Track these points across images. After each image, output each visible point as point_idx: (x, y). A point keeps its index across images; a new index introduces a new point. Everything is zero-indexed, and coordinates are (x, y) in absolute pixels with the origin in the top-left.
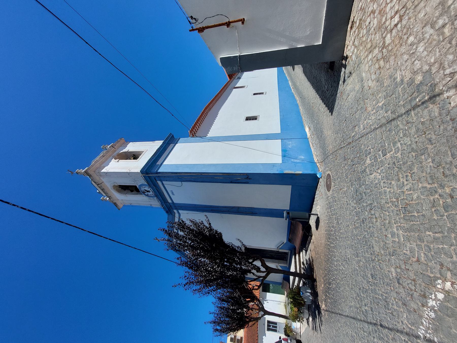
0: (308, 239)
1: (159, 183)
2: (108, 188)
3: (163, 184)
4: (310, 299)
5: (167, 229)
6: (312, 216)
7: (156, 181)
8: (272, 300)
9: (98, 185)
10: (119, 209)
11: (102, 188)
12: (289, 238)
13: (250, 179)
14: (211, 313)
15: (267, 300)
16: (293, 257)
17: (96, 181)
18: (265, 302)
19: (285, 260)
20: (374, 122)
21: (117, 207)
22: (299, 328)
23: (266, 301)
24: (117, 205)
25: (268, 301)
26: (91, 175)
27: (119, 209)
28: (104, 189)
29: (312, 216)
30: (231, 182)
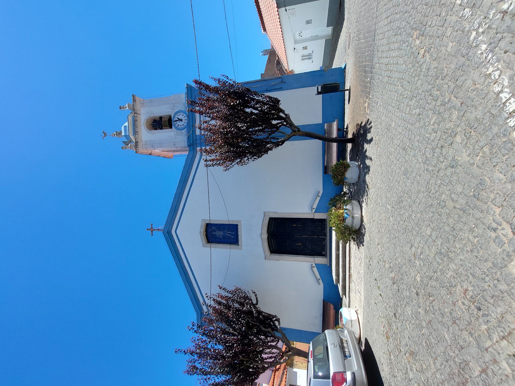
10: (136, 152)
11: (136, 119)
17: (136, 109)
24: (138, 145)
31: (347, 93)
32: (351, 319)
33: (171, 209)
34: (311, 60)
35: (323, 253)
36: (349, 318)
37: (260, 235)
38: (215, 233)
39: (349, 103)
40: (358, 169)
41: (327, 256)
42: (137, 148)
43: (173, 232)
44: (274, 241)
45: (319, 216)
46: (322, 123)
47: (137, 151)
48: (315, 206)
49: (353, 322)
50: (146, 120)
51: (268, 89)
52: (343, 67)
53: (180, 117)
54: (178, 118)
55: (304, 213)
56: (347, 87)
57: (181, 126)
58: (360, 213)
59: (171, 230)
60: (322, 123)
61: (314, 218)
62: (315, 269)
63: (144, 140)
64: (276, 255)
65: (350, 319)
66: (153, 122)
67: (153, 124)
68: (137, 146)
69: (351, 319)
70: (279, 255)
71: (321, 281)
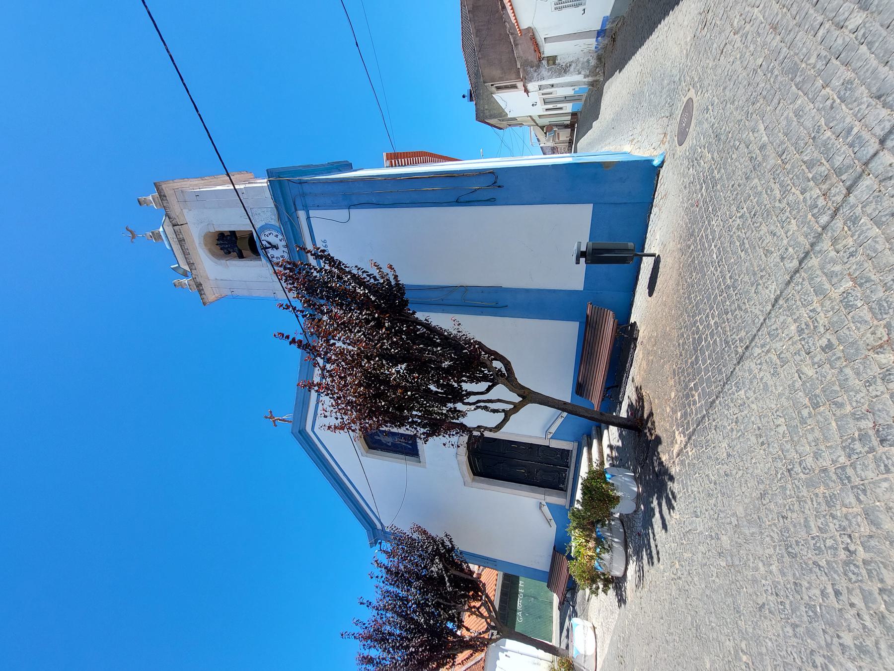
0: (626, 366)
1: (302, 214)
2: (194, 241)
3: (308, 218)
4: (633, 490)
5: (299, 337)
6: (644, 258)
7: (296, 210)
8: (520, 651)
9: (174, 225)
10: (204, 304)
11: (181, 236)
12: (578, 380)
13: (499, 187)
14: (361, 603)
15: (507, 651)
16: (585, 450)
17: (173, 215)
18: (500, 654)
19: (562, 489)
20: (741, 438)
21: (201, 295)
22: (593, 654)
23: (503, 651)
24: (203, 289)
25: (508, 653)
26: (165, 196)
27: (204, 304)
28: (184, 240)
29: (644, 258)
30: (458, 202)
31: (647, 265)
32: (585, 652)
33: (296, 404)
34: (581, 8)
35: (561, 486)
36: (582, 652)
37: (455, 454)
38: (378, 438)
39: (650, 294)
40: (635, 505)
41: (566, 491)
42: (204, 296)
43: (308, 429)
44: (478, 462)
45: (555, 444)
46: (584, 259)
47: (206, 300)
48: (553, 430)
49: (587, 658)
50: (203, 238)
51: (461, 199)
52: (656, 163)
53: (273, 239)
54: (269, 243)
55: (530, 437)
56: (653, 245)
57: (277, 258)
58: (623, 569)
59: (305, 427)
60: (584, 259)
61: (548, 447)
62: (546, 509)
63: (212, 276)
64: (482, 482)
65: (584, 653)
66: (218, 240)
67: (220, 244)
68: (203, 292)
69: (585, 652)
70: (488, 483)
71: (553, 523)
